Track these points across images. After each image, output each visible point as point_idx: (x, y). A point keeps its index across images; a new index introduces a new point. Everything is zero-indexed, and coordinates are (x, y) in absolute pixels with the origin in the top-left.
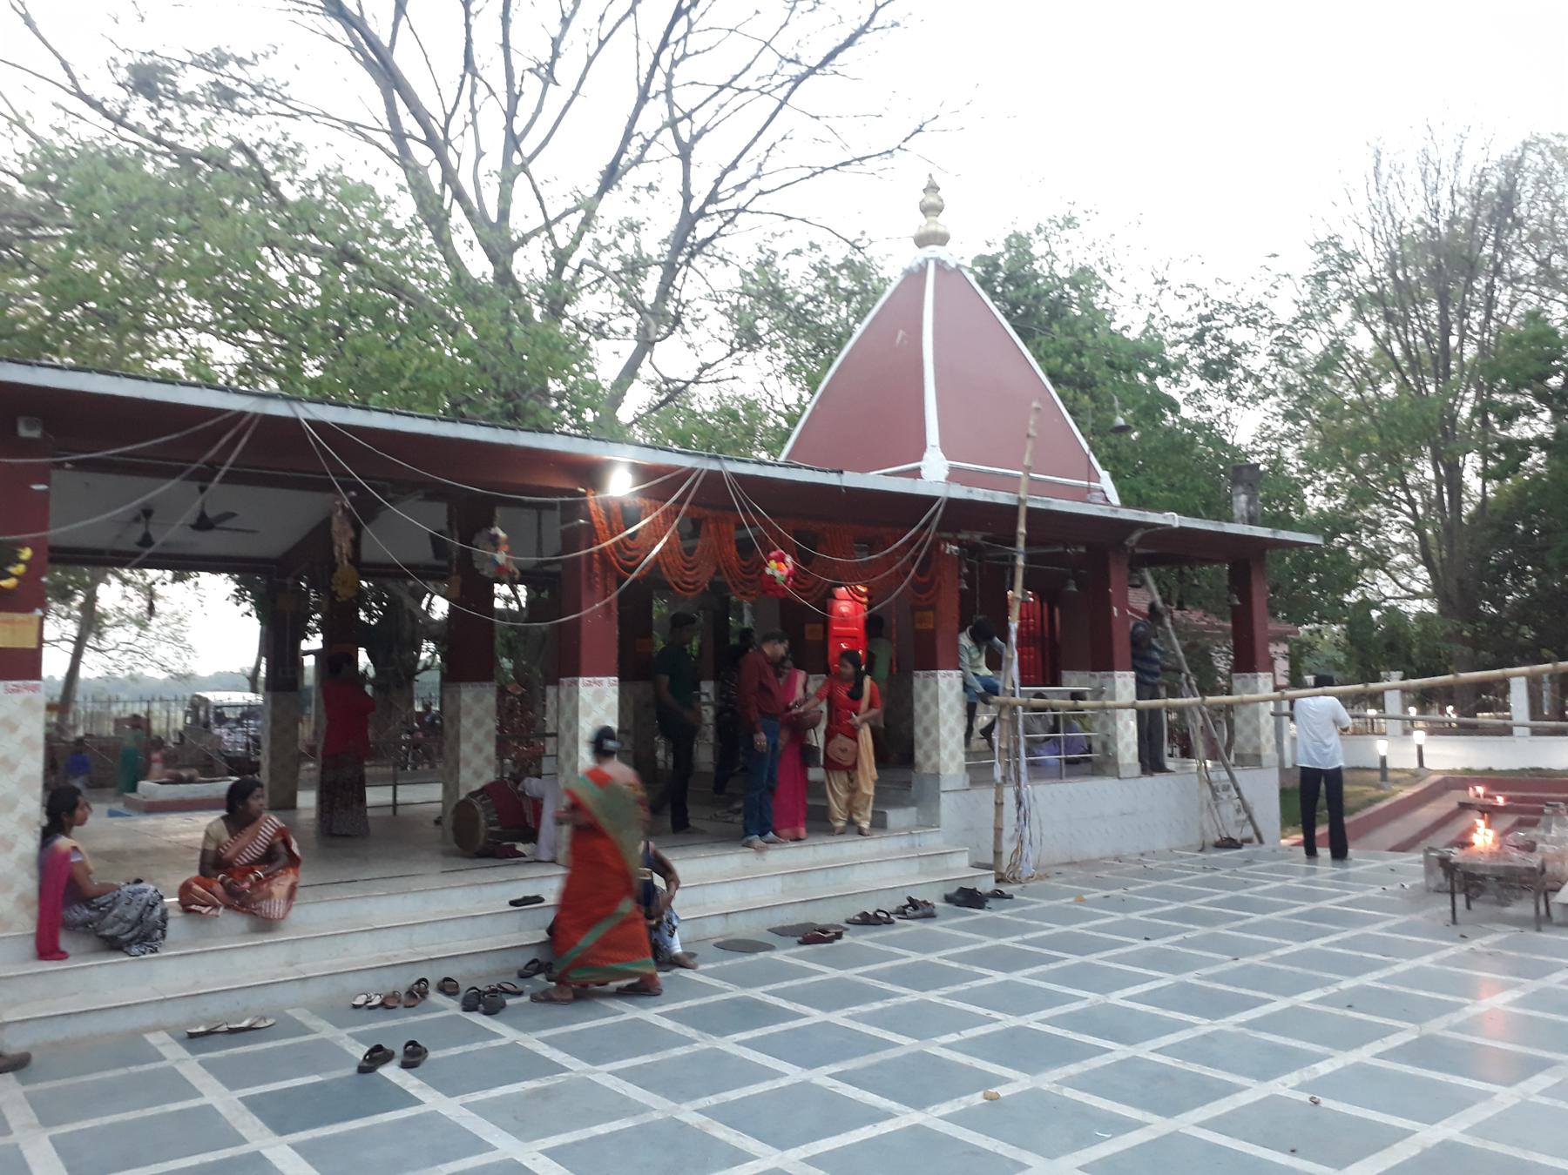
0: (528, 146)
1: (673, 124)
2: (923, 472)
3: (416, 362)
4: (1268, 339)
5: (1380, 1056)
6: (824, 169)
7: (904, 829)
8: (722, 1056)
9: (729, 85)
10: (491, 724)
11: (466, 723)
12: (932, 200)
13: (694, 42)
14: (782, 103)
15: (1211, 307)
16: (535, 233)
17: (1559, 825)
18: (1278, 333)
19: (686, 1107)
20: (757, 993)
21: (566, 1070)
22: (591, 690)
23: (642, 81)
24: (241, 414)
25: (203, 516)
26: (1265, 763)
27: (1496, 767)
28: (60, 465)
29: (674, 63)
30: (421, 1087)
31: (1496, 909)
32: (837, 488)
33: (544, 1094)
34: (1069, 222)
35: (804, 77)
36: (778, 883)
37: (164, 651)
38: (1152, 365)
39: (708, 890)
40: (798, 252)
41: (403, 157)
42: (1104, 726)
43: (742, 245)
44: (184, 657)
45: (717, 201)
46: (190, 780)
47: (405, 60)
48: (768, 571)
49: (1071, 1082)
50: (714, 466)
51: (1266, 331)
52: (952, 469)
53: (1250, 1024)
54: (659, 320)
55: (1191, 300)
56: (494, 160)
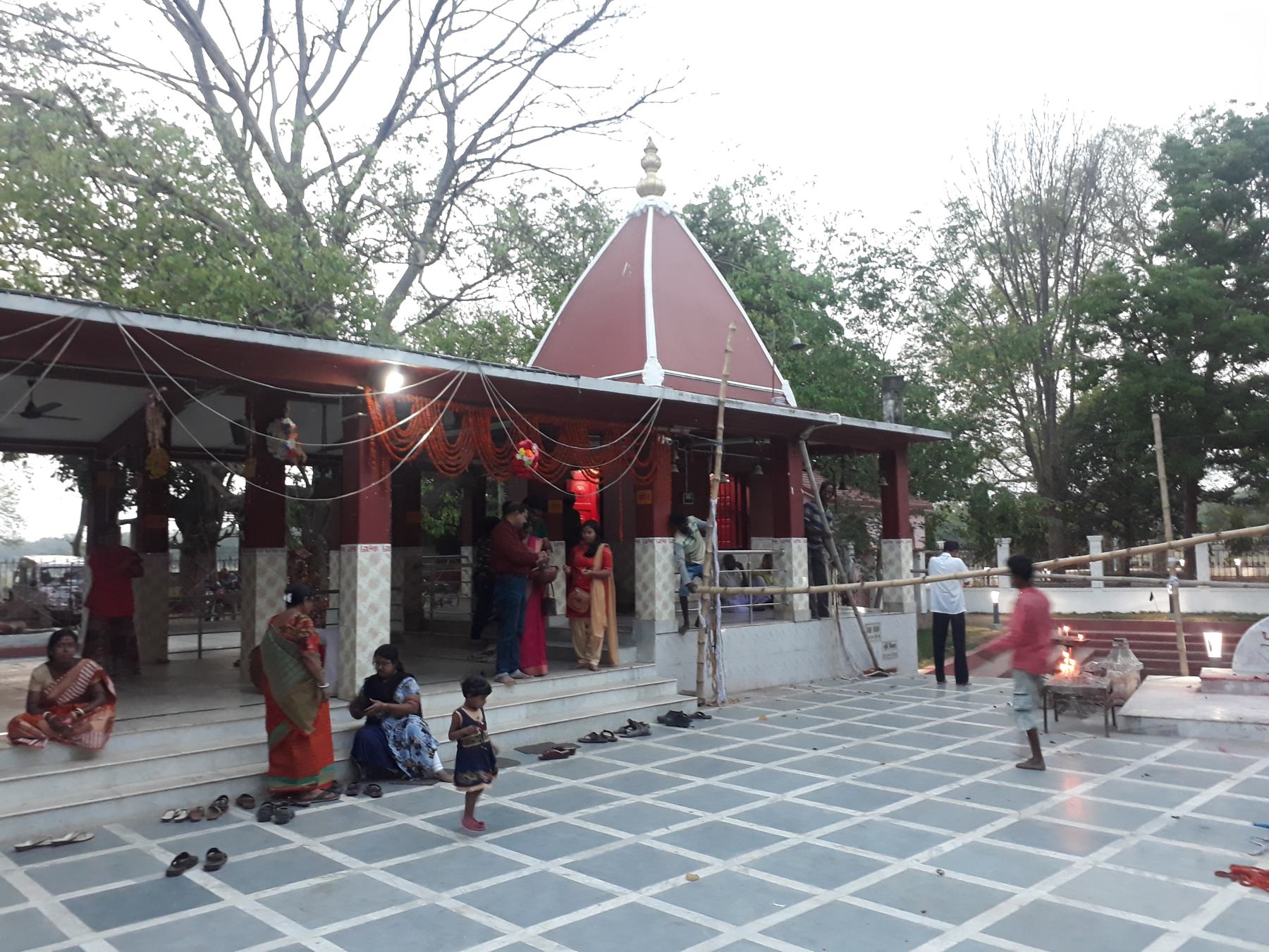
0: (317, 101)
1: (440, 87)
2: (644, 378)
9: (487, 57)
11: (261, 582)
12: (651, 158)
13: (458, 21)
16: (323, 172)
18: (919, 273)
19: (446, 895)
27: (1079, 612)
29: (442, 37)
30: (219, 886)
31: (1078, 720)
32: (576, 389)
33: (320, 888)
34: (760, 180)
38: (823, 296)
40: (544, 196)
41: (210, 106)
43: (497, 188)
44: (14, 527)
46: (18, 631)
48: (518, 457)
49: (756, 865)
50: (473, 370)
51: (910, 271)
52: (666, 375)
54: (426, 249)
55: (853, 246)
56: (288, 111)
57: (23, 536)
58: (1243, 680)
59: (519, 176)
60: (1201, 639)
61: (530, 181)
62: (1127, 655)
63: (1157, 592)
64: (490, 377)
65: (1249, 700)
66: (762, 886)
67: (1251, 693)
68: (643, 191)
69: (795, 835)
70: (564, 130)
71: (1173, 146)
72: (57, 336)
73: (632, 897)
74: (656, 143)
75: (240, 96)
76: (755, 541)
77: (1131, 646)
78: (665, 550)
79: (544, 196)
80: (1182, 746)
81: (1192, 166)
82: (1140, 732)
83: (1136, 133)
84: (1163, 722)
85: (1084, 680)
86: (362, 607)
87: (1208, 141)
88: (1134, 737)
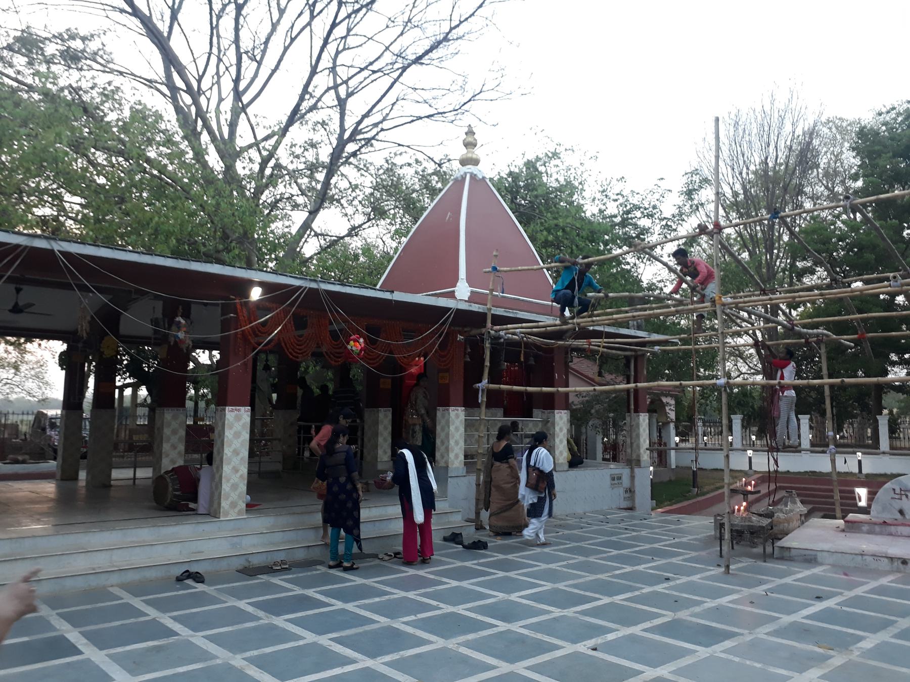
0: (246, 99)
1: (336, 87)
2: (456, 294)
3: (156, 219)
4: (659, 226)
5: (645, 630)
6: (421, 118)
8: (274, 627)
9: (366, 68)
11: (167, 431)
12: (470, 139)
13: (351, 41)
14: (396, 81)
15: (628, 207)
16: (250, 146)
17: (792, 503)
18: (664, 223)
19: (239, 657)
21: (177, 634)
22: (233, 414)
23: (313, 63)
24: (18, 246)
26: (642, 464)
27: (791, 471)
29: (338, 53)
30: (85, 644)
31: (748, 549)
32: (391, 300)
33: (158, 649)
34: (555, 155)
35: (409, 65)
37: (30, 385)
38: (607, 237)
40: (409, 165)
41: (174, 100)
43: (376, 157)
44: (43, 389)
45: (360, 132)
46: (24, 462)
47: (177, 44)
49: (467, 644)
50: (313, 285)
51: (657, 221)
52: (472, 292)
53: (584, 613)
54: (322, 198)
56: (227, 105)
57: (49, 396)
58: (875, 524)
59: (393, 150)
60: (853, 492)
61: (401, 154)
62: (795, 503)
63: (849, 457)
65: (879, 539)
66: (465, 660)
67: (881, 534)
68: (464, 162)
69: (504, 624)
70: (421, 118)
71: (862, 133)
72: (9, 258)
73: (369, 663)
75: (195, 95)
76: (536, 412)
77: (799, 495)
79: (409, 165)
80: (817, 570)
81: (877, 148)
82: (791, 559)
83: (844, 124)
84: (807, 552)
85: (750, 520)
87: (890, 130)
88: (786, 562)
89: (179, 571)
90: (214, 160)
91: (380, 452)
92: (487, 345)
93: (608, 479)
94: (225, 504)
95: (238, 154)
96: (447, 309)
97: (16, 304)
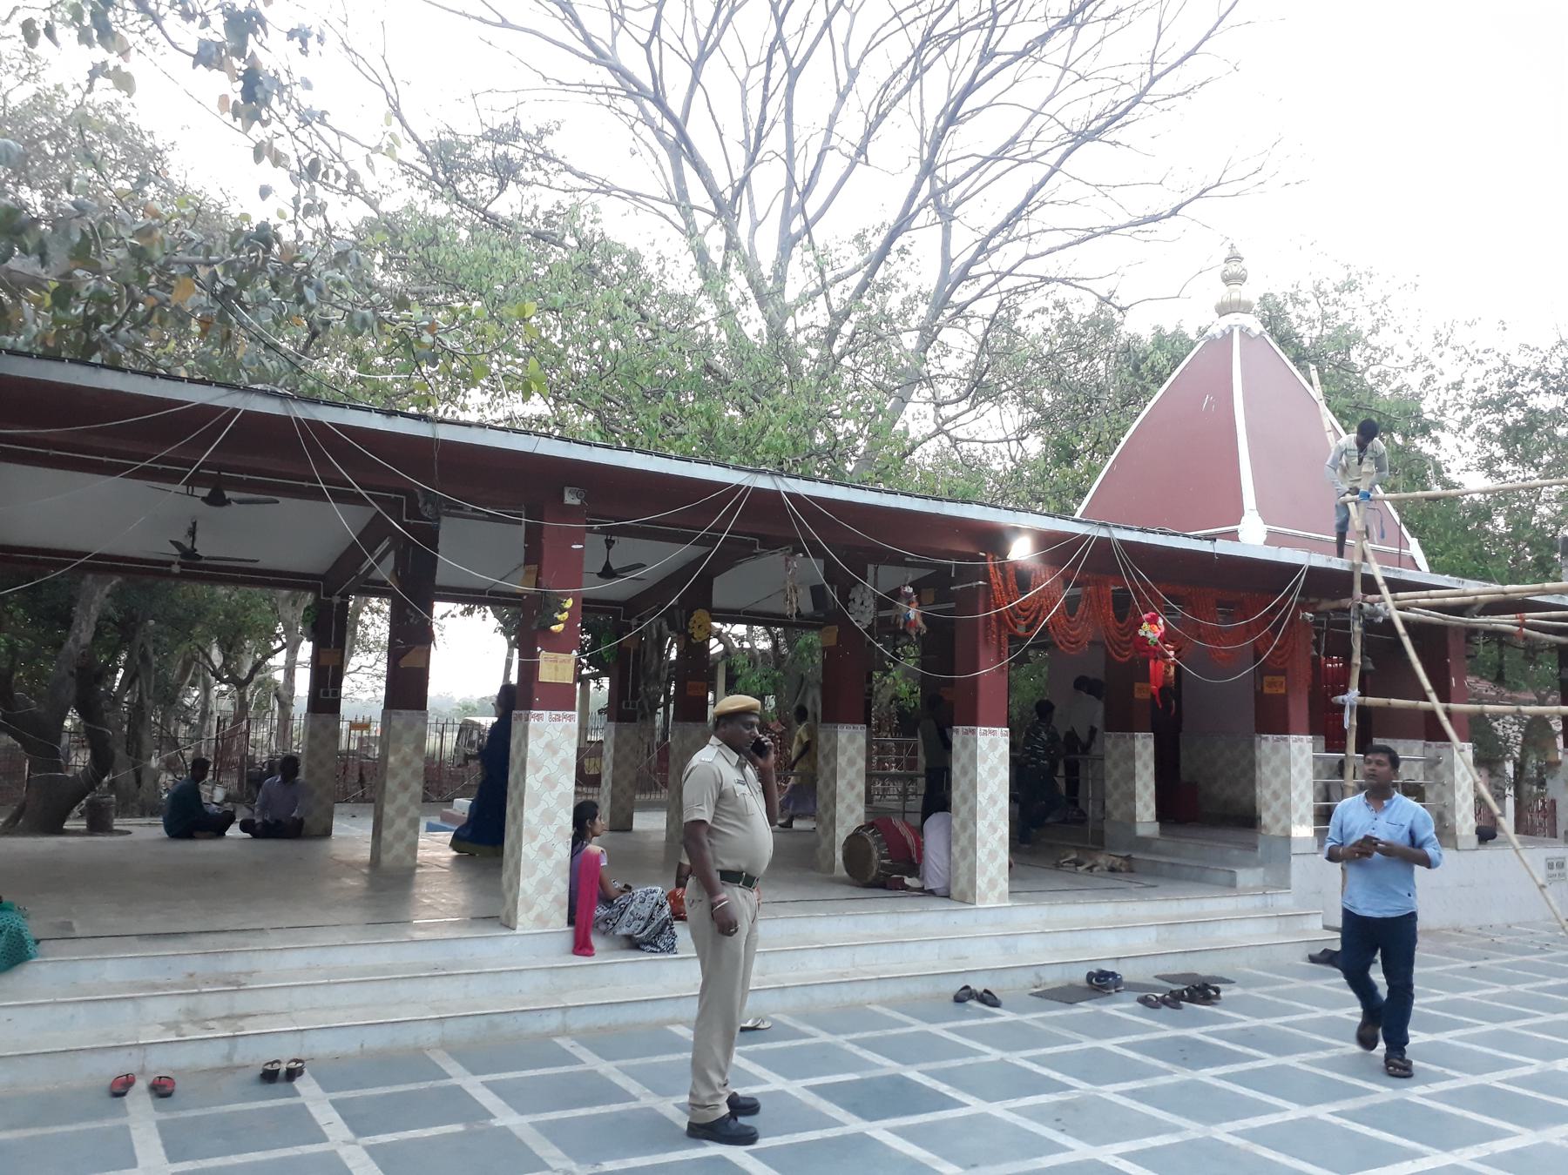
7: (1254, 888)
8: (1207, 1089)
10: (861, 764)
12: (1234, 268)
20: (1018, 1058)
25: (607, 566)
28: (590, 530)
36: (1153, 933)
39: (1094, 935)
40: (1044, 311)
41: (690, 231)
42: (1440, 796)
48: (1141, 633)
50: (1103, 533)
52: (1269, 532)
55: (1489, 366)
64: (1121, 541)
74: (1241, 250)
78: (993, 746)
79: (1044, 311)
86: (982, 797)
89: (956, 986)
90: (753, 324)
91: (1139, 806)
92: (1357, 628)
93: (1543, 866)
94: (981, 882)
95: (787, 311)
96: (1296, 568)
97: (607, 566)
